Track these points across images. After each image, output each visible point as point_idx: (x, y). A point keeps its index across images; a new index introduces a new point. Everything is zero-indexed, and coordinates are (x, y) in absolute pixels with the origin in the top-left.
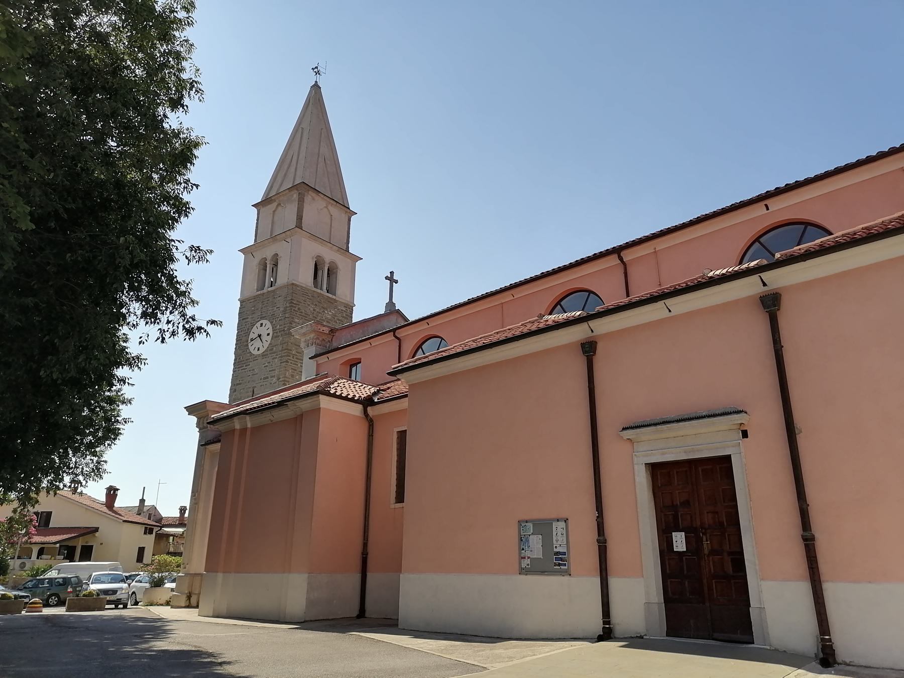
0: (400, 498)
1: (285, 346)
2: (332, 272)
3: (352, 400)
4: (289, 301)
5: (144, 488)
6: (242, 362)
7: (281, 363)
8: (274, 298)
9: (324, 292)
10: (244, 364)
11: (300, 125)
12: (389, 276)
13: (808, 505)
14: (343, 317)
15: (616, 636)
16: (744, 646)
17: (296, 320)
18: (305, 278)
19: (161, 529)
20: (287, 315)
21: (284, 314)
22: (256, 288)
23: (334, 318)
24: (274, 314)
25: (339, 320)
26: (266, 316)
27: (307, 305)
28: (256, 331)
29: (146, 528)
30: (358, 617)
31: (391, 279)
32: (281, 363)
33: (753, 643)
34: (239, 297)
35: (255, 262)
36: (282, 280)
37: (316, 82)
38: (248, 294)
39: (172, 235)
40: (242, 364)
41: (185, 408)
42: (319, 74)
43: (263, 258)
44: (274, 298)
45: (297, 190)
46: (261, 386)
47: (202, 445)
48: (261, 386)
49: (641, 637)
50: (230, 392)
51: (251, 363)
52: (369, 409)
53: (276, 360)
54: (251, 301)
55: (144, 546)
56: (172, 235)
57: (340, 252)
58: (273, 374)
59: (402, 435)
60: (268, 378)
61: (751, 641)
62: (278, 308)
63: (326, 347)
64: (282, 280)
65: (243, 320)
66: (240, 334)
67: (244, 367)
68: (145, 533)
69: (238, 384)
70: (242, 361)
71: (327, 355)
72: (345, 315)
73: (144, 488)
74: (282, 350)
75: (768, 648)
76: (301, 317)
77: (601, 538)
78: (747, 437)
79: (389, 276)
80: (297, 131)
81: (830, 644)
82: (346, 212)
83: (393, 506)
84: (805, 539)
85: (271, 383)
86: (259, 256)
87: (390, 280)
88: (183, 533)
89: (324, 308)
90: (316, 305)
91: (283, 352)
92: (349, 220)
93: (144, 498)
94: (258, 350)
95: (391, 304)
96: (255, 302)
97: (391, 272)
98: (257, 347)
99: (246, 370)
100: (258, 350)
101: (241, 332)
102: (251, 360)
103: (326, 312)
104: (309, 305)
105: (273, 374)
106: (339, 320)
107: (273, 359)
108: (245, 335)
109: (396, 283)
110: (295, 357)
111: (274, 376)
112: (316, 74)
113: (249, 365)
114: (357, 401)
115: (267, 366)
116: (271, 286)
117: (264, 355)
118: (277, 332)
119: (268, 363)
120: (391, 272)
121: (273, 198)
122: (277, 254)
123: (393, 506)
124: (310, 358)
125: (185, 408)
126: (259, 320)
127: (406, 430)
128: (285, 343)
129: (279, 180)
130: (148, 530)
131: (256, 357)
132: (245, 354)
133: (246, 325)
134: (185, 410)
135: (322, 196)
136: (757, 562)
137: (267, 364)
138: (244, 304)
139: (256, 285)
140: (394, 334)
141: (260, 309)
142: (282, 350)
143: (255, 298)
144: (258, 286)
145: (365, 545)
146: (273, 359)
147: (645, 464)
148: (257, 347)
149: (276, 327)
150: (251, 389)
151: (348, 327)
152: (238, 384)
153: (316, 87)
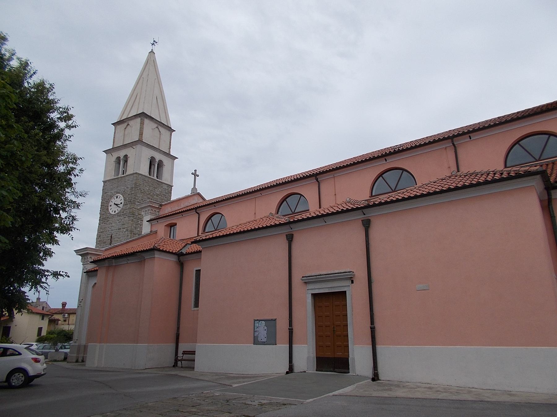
0: (197, 305)
2: (160, 164)
3: (172, 253)
4: (134, 184)
9: (155, 178)
11: (141, 76)
12: (194, 173)
13: (374, 314)
14: (166, 193)
15: (295, 372)
16: (345, 374)
17: (138, 195)
18: (144, 169)
19: (52, 316)
22: (113, 174)
23: (161, 194)
24: (125, 191)
25: (164, 195)
28: (114, 200)
30: (174, 366)
31: (195, 175)
33: (349, 373)
35: (114, 158)
36: (130, 171)
37: (152, 50)
41: (74, 251)
42: (154, 45)
43: (118, 157)
47: (85, 272)
49: (305, 372)
50: (97, 237)
52: (181, 257)
53: (126, 218)
55: (42, 327)
58: (124, 226)
59: (198, 272)
60: (120, 229)
61: (348, 372)
63: (156, 214)
64: (130, 171)
65: (105, 193)
66: (103, 201)
67: (106, 222)
69: (102, 232)
71: (157, 220)
72: (167, 192)
75: (354, 374)
76: (141, 193)
77: (290, 328)
78: (353, 283)
79: (194, 173)
80: (140, 79)
81: (377, 372)
83: (193, 309)
84: (371, 328)
87: (195, 175)
89: (155, 188)
90: (150, 186)
92: (171, 135)
94: (115, 212)
95: (194, 189)
97: (195, 170)
98: (113, 210)
99: (107, 224)
100: (115, 212)
103: (156, 190)
105: (124, 226)
106: (164, 195)
108: (105, 198)
109: (198, 176)
110: (135, 217)
112: (152, 45)
113: (109, 221)
114: (175, 254)
115: (120, 222)
116: (123, 174)
117: (118, 215)
118: (126, 202)
120: (195, 170)
121: (124, 121)
122: (127, 155)
123: (193, 309)
124: (147, 221)
125: (74, 251)
126: (115, 194)
127: (200, 270)
129: (128, 109)
130: (43, 316)
136: (353, 338)
137: (120, 221)
139: (113, 173)
140: (196, 211)
142: (129, 213)
144: (115, 174)
145: (178, 328)
147: (311, 294)
148: (113, 210)
149: (126, 199)
151: (169, 203)
152: (102, 232)
153: (152, 52)
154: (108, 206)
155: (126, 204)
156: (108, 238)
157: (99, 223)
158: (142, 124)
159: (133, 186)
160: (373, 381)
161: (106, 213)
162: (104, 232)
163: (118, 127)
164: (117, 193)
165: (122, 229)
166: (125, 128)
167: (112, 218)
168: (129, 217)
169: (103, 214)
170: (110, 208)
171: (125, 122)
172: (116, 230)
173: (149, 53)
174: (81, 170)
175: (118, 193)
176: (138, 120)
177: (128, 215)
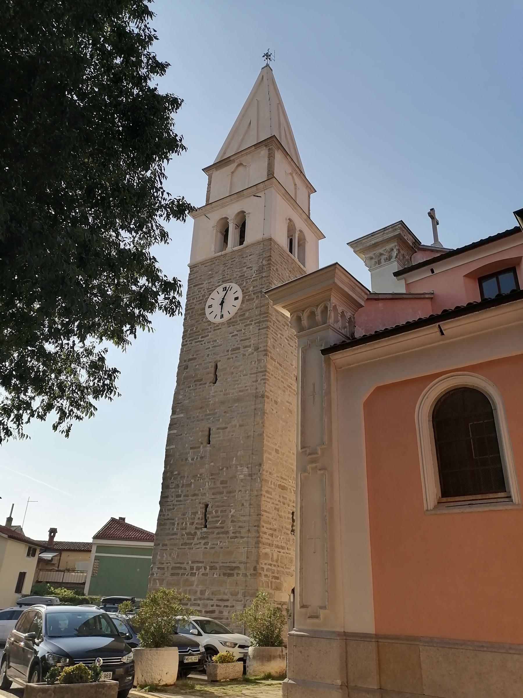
1: (263, 309)
5: (13, 505)
6: (197, 334)
7: (259, 329)
8: (243, 257)
10: (199, 335)
20: (264, 274)
21: (260, 273)
26: (231, 279)
27: (283, 268)
29: (30, 548)
32: (259, 329)
34: (188, 262)
38: (201, 257)
39: (172, 115)
40: (197, 335)
44: (243, 257)
45: (266, 146)
46: (228, 359)
48: (228, 359)
51: (210, 334)
53: (251, 327)
54: (207, 264)
56: (172, 115)
57: (307, 223)
58: (247, 343)
62: (249, 268)
65: (194, 286)
66: (191, 301)
67: (200, 339)
68: (28, 555)
69: (190, 360)
70: (196, 332)
73: (13, 505)
74: (260, 315)
82: (307, 186)
85: (244, 355)
86: (216, 216)
88: (52, 559)
91: (262, 316)
93: (12, 517)
96: (213, 266)
101: (194, 299)
102: (209, 330)
104: (285, 269)
105: (247, 343)
107: (245, 326)
111: (250, 346)
113: (208, 336)
117: (231, 322)
119: (237, 331)
121: (231, 159)
126: (220, 284)
128: (263, 306)
131: (217, 326)
132: (200, 324)
133: (199, 291)
134: (352, 250)
135: (290, 160)
137: (236, 333)
138: (195, 269)
141: (220, 272)
142: (260, 315)
143: (212, 261)
144: (215, 249)
146: (245, 326)
149: (247, 289)
150: (213, 364)
152: (190, 360)
154: (204, 309)
155: (248, 300)
156: (208, 370)
157: (183, 342)
158: (271, 157)
159: (264, 262)
160: (113, 520)
161: (200, 321)
162: (195, 359)
163: (217, 174)
164: (223, 282)
165: (242, 349)
166: (233, 173)
167: (214, 330)
168: (258, 323)
169: (193, 325)
170: (208, 311)
171: (234, 161)
172: (228, 351)
173: (262, 68)
174: (111, 398)
175: (227, 280)
176: (264, 152)
177: (256, 320)
